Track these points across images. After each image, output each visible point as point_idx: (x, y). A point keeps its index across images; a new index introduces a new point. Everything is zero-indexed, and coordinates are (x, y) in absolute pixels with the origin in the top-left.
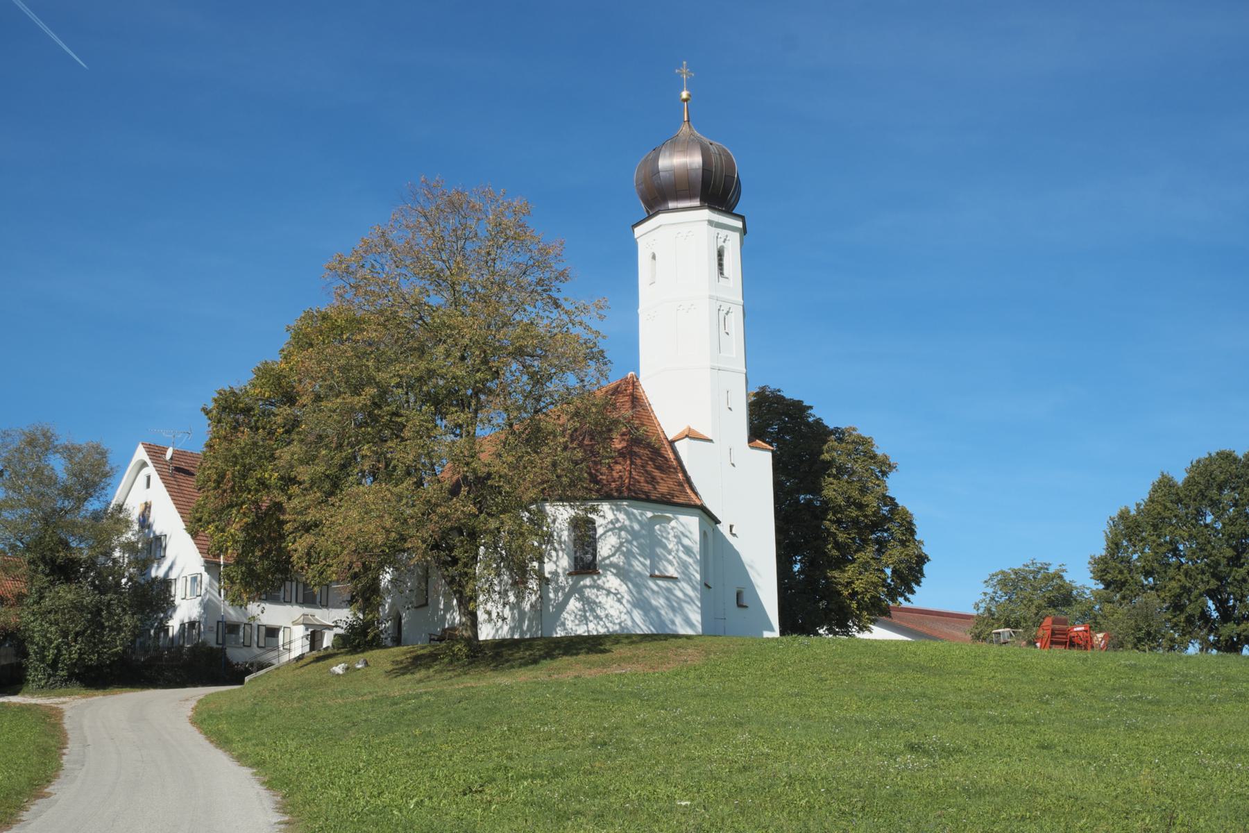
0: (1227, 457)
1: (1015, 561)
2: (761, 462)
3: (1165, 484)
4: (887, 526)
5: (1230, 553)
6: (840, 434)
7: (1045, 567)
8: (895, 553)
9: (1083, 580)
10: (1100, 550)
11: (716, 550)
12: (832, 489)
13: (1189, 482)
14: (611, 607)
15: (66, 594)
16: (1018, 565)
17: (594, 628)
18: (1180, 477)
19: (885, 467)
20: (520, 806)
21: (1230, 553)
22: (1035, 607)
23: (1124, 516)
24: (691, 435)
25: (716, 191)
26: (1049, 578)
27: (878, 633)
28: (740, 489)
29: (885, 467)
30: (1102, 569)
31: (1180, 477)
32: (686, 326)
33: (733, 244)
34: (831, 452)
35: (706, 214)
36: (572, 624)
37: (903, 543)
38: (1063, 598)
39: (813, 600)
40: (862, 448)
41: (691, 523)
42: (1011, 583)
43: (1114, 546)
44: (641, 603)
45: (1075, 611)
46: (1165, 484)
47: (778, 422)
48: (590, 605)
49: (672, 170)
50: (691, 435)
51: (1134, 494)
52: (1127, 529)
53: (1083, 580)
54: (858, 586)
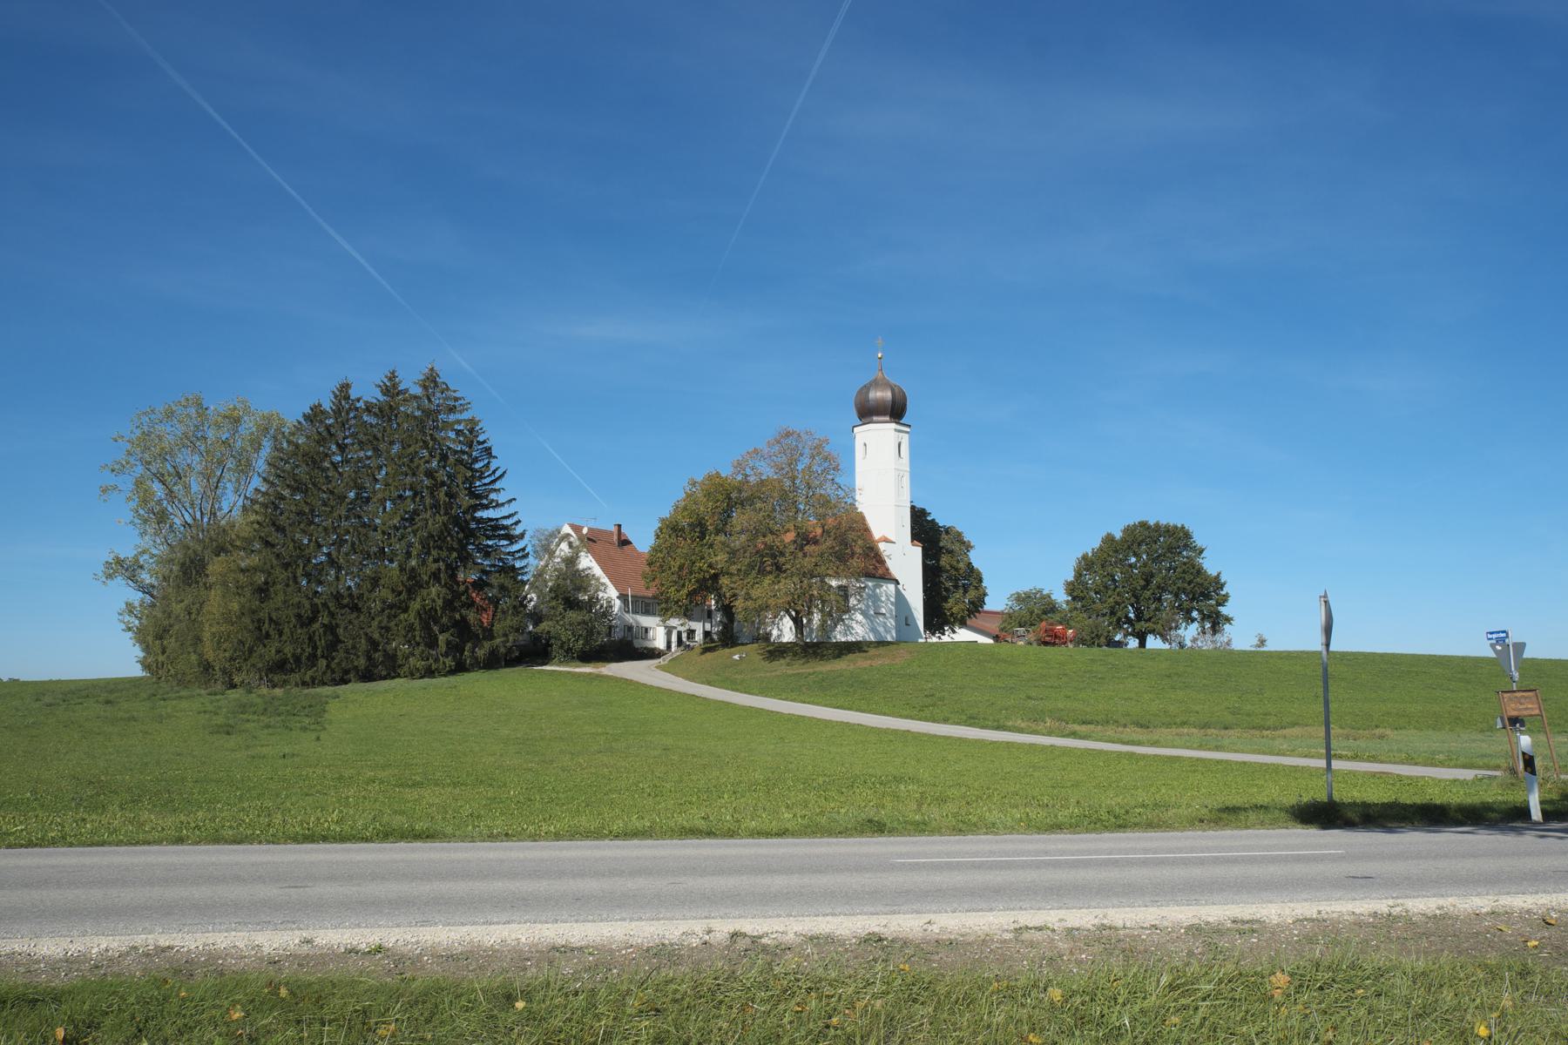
0: (1144, 525)
1: (1025, 587)
2: (917, 552)
3: (1109, 539)
4: (972, 578)
5: (1143, 583)
6: (947, 531)
7: (1040, 591)
8: (972, 594)
9: (1061, 597)
10: (1071, 578)
11: (900, 600)
12: (945, 561)
13: (1123, 540)
14: (857, 628)
15: (573, 615)
16: (1027, 589)
17: (851, 639)
18: (1118, 535)
19: (968, 547)
20: (37, 705)
21: (1143, 583)
22: (1034, 614)
23: (1085, 557)
24: (887, 540)
25: (896, 411)
26: (1043, 597)
27: (963, 635)
28: (906, 563)
29: (968, 547)
30: (1071, 588)
31: (1118, 535)
32: (881, 480)
33: (905, 439)
34: (945, 542)
35: (893, 426)
36: (839, 636)
37: (976, 588)
38: (1050, 608)
39: (937, 618)
40: (959, 538)
41: (892, 587)
42: (1022, 598)
43: (1079, 575)
44: (874, 630)
45: (1057, 617)
46: (1109, 539)
47: (924, 529)
48: (849, 628)
49: (876, 400)
50: (887, 540)
51: (1091, 543)
52: (1087, 564)
53: (1061, 597)
54: (955, 610)
